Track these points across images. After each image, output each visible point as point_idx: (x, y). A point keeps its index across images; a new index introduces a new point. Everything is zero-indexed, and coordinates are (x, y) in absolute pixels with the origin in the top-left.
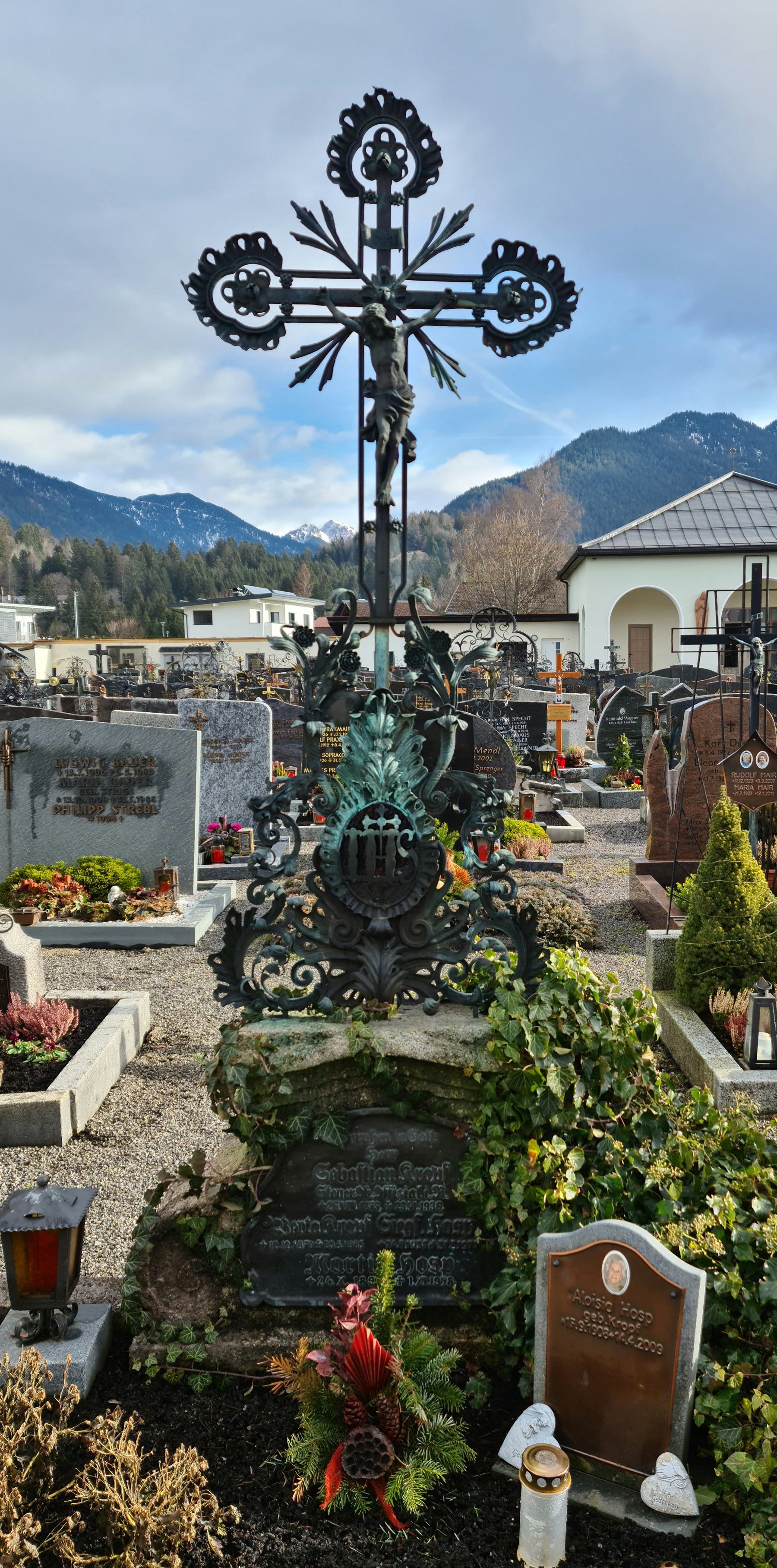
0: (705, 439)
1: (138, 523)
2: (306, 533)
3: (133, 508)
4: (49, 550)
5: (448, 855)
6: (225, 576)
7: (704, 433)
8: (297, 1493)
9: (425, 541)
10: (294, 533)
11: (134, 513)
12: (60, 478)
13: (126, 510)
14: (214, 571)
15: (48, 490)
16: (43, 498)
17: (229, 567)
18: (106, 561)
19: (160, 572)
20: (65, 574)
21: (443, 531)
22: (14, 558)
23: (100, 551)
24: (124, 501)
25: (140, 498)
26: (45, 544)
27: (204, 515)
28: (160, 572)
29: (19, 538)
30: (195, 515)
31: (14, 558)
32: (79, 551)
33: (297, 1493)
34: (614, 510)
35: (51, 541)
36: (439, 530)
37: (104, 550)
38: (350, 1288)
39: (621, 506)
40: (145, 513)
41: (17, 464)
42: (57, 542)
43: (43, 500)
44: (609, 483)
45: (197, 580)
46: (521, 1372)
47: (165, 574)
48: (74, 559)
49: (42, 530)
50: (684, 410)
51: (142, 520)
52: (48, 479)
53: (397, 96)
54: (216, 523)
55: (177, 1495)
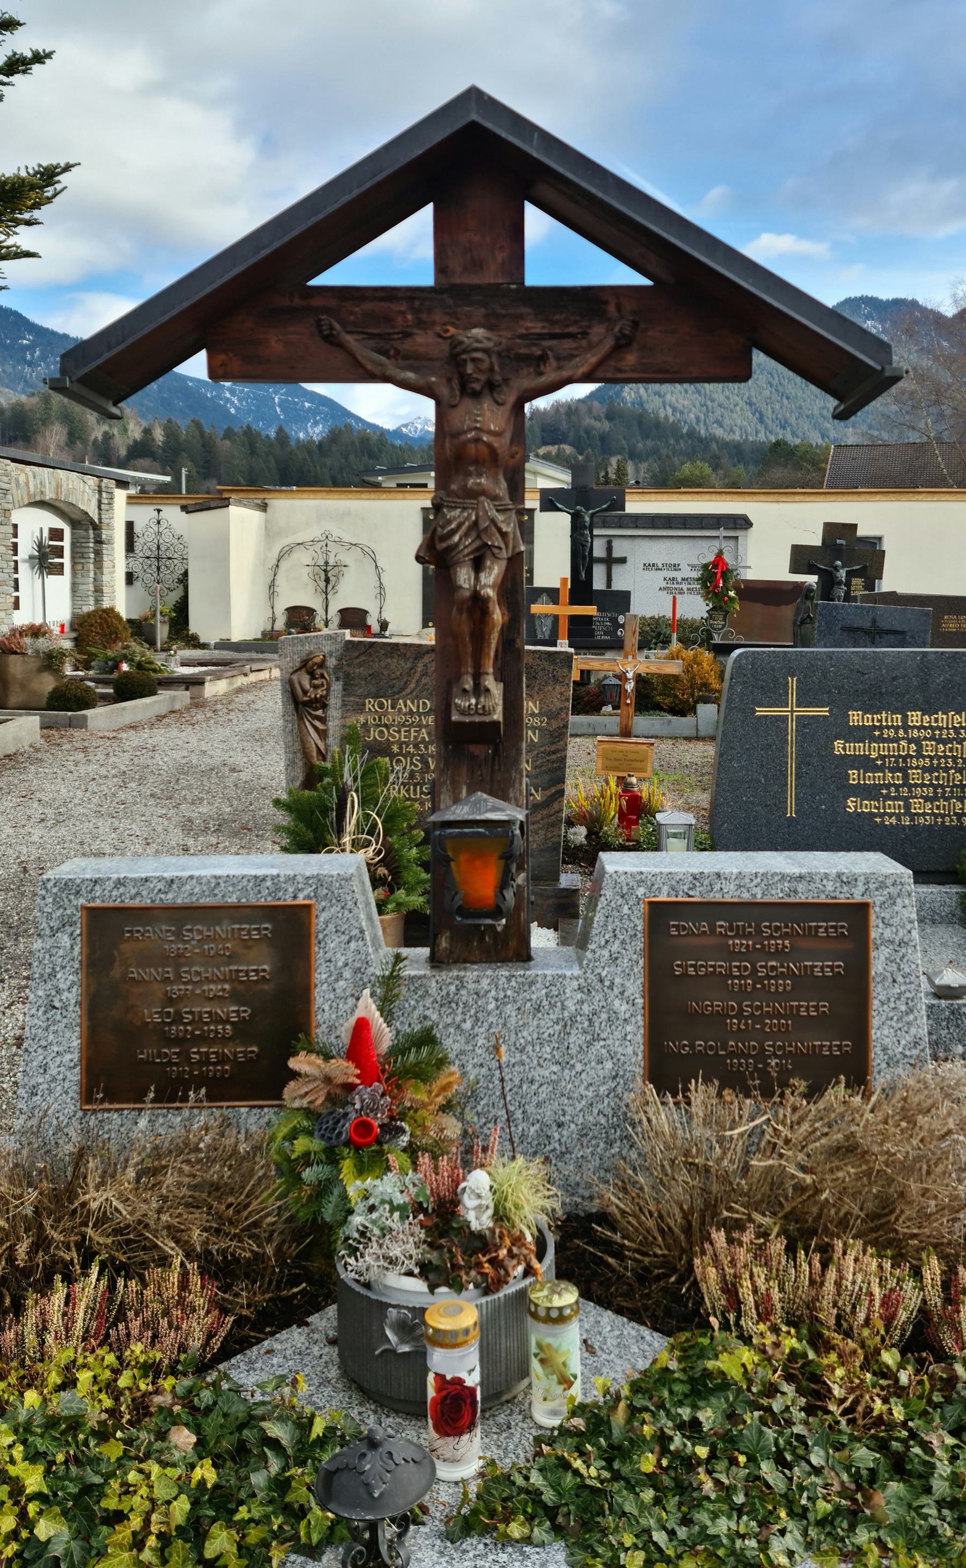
0: (883, 327)
1: (233, 411)
2: (419, 426)
3: (228, 395)
4: (135, 432)
6: (341, 469)
7: (882, 321)
9: (572, 434)
10: (406, 426)
11: (228, 400)
14: (328, 461)
17: (346, 458)
18: (204, 446)
20: (155, 459)
21: (593, 422)
22: (96, 439)
23: (197, 434)
26: (131, 426)
27: (307, 405)
30: (297, 404)
31: (96, 439)
34: (777, 407)
35: (138, 423)
36: (588, 421)
37: (202, 433)
39: (785, 401)
40: (240, 400)
42: (145, 424)
44: (772, 376)
45: (309, 471)
46: (293, 1063)
47: (272, 464)
50: (859, 295)
54: (320, 413)
55: (24, 983)
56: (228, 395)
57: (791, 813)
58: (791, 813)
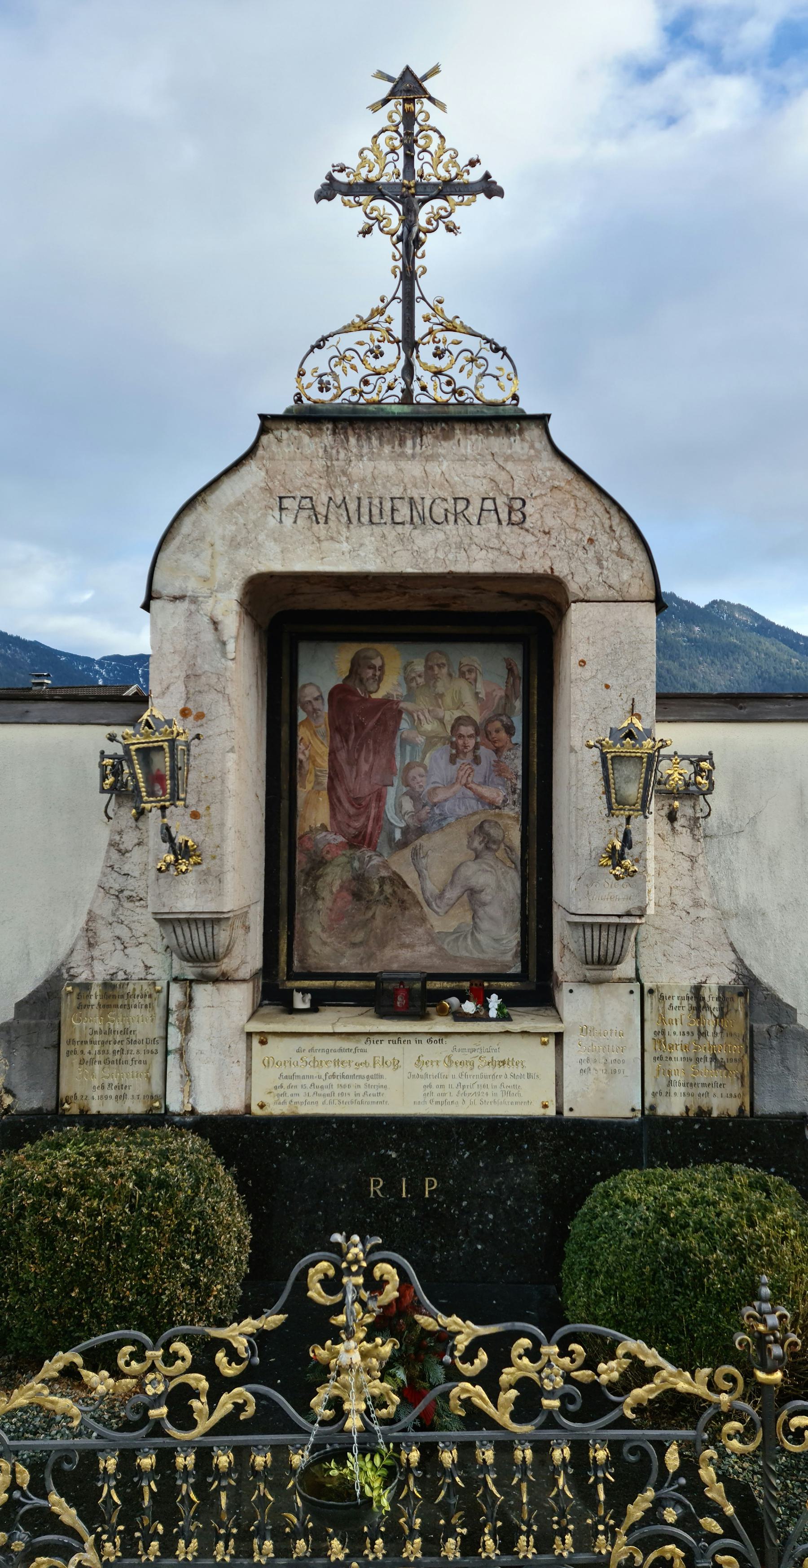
3: (97, 667)
13: (89, 669)
15: (10, 648)
24: (89, 661)
25: (104, 658)
40: (108, 672)
52: (11, 637)
56: (97, 667)
57: (404, 1180)
58: (404, 1180)
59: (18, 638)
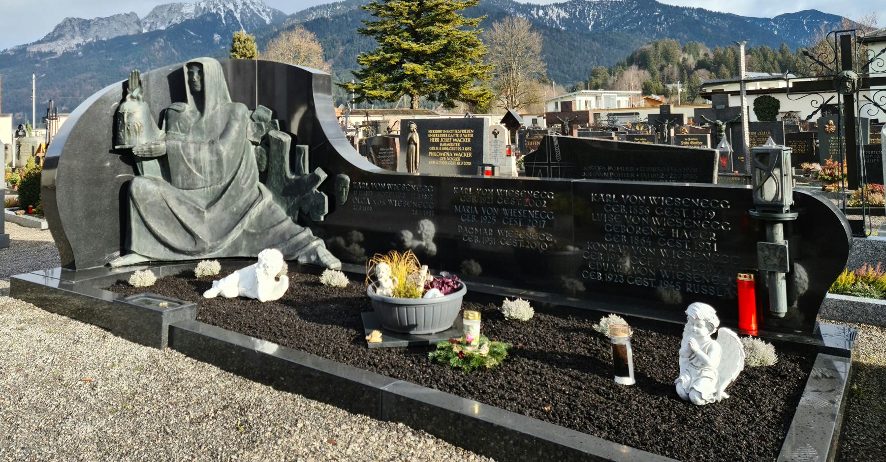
5: (143, 121)
8: (470, 164)
11: (773, 27)
12: (722, 12)
13: (767, 25)
16: (711, 25)
19: (772, 63)
24: (766, 20)
25: (777, 17)
28: (772, 63)
29: (684, 50)
32: (717, 55)
33: (470, 164)
38: (755, 213)
40: (781, 26)
41: (696, 7)
43: (712, 26)
48: (715, 60)
49: (699, 45)
51: (779, 31)
52: (715, 13)
53: (366, 158)
59: (719, 13)
